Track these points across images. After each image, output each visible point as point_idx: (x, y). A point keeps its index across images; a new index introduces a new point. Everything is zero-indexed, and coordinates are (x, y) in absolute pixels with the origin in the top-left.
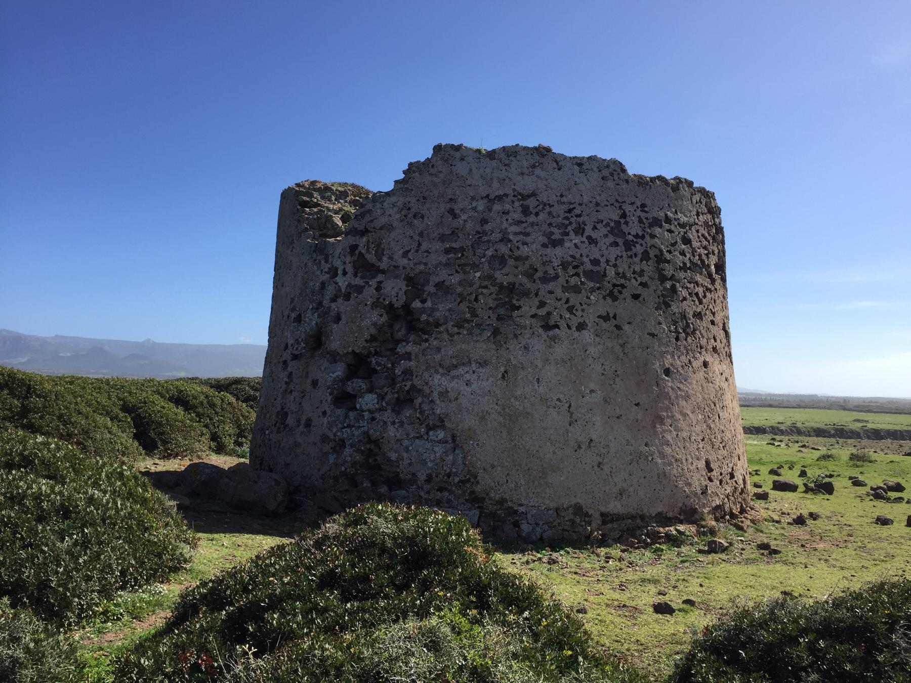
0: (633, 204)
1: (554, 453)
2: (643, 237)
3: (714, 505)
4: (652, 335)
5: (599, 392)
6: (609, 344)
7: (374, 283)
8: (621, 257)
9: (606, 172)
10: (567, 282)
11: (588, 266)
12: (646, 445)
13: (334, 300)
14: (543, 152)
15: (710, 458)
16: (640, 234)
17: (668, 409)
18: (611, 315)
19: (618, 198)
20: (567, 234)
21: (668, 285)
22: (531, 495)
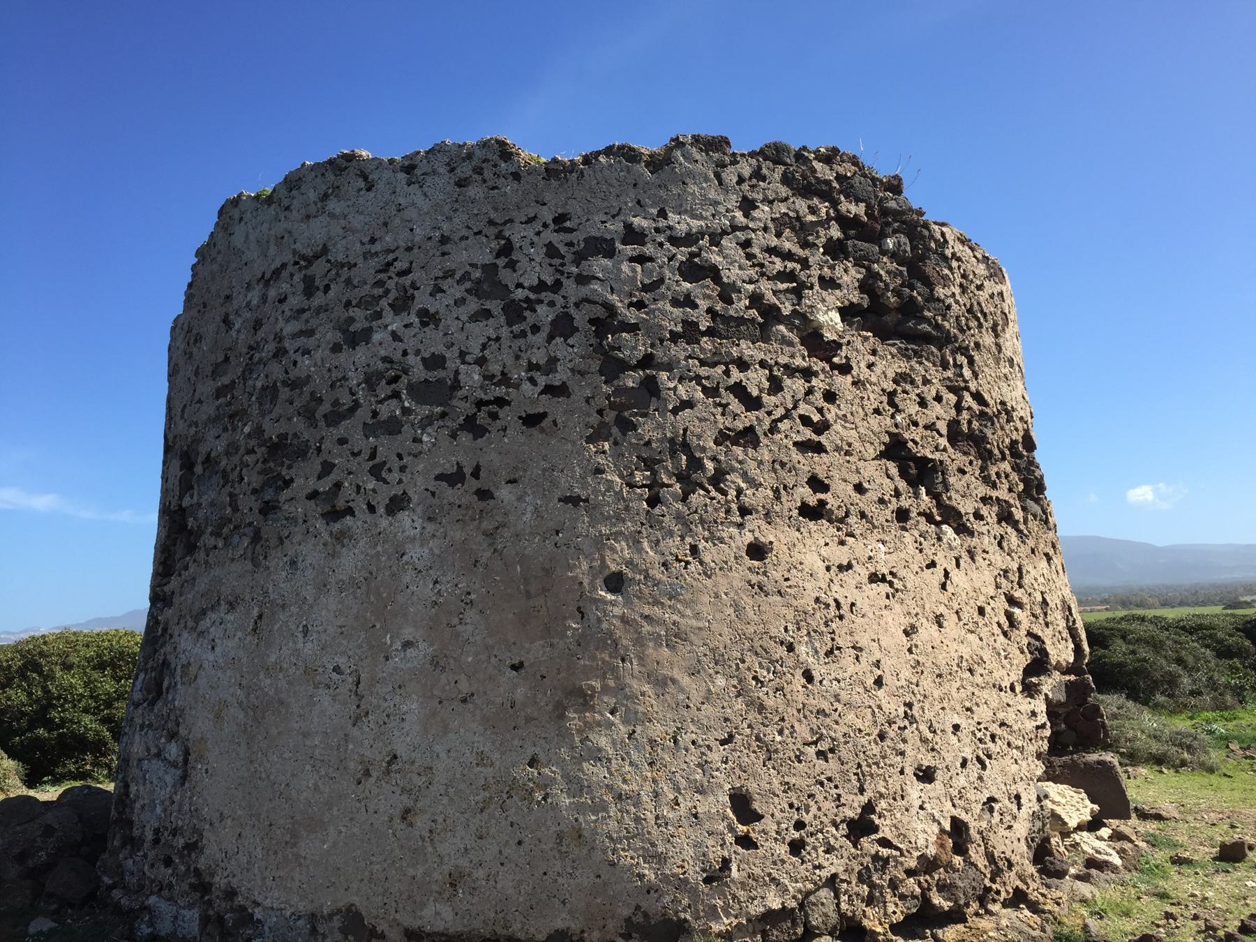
0: (530, 221)
1: (316, 788)
2: (557, 285)
3: (756, 909)
4: (574, 501)
5: (422, 645)
6: (458, 535)
8: (498, 339)
9: (465, 170)
10: (375, 414)
11: (419, 372)
12: (533, 763)
14: (344, 164)
15: (752, 786)
16: (549, 281)
17: (607, 670)
18: (468, 470)
19: (493, 215)
20: (378, 315)
21: (631, 380)
22: (269, 883)
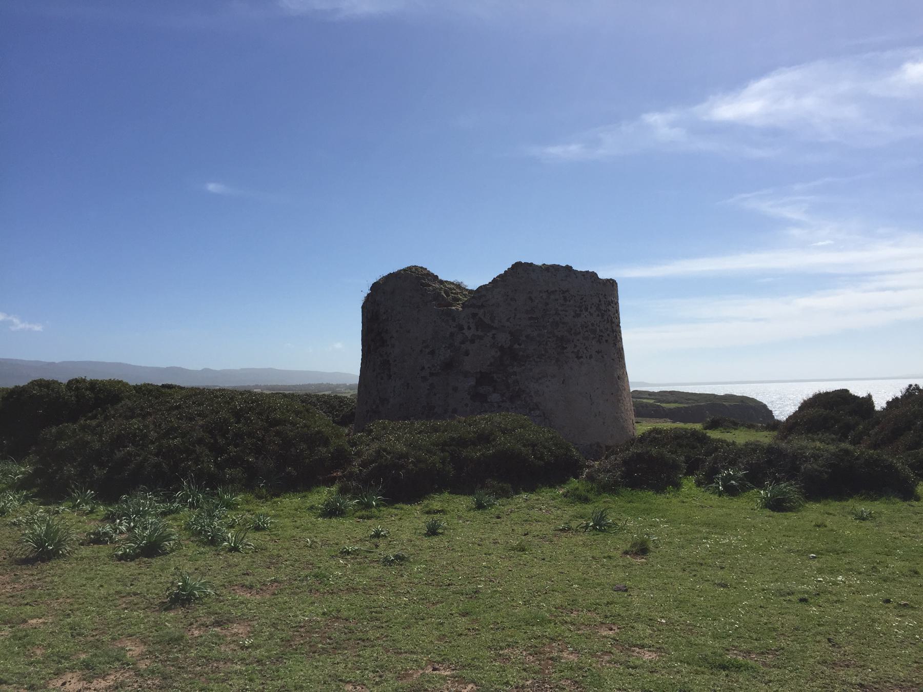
7: (490, 334)
13: (463, 343)
